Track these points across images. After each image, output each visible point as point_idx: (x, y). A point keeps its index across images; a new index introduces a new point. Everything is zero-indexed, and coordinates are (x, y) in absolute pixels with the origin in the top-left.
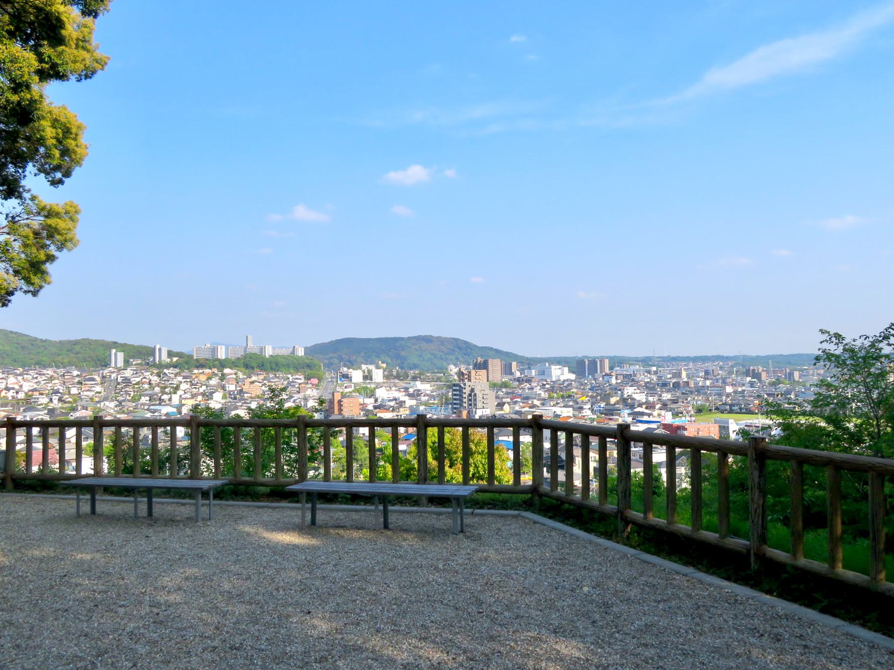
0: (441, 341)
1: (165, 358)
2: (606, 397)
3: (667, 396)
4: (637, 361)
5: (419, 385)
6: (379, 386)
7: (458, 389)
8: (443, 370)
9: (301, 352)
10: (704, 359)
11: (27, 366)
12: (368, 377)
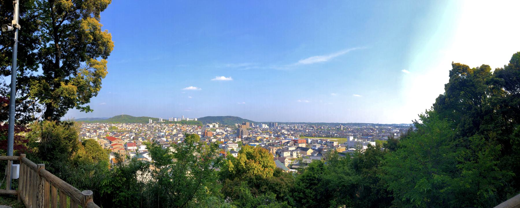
0: (233, 117)
1: (162, 121)
2: (277, 133)
3: (292, 132)
4: (284, 123)
5: (228, 129)
6: (217, 129)
7: (238, 130)
8: (234, 125)
9: (196, 120)
10: (301, 123)
11: (131, 123)
12: (214, 126)
